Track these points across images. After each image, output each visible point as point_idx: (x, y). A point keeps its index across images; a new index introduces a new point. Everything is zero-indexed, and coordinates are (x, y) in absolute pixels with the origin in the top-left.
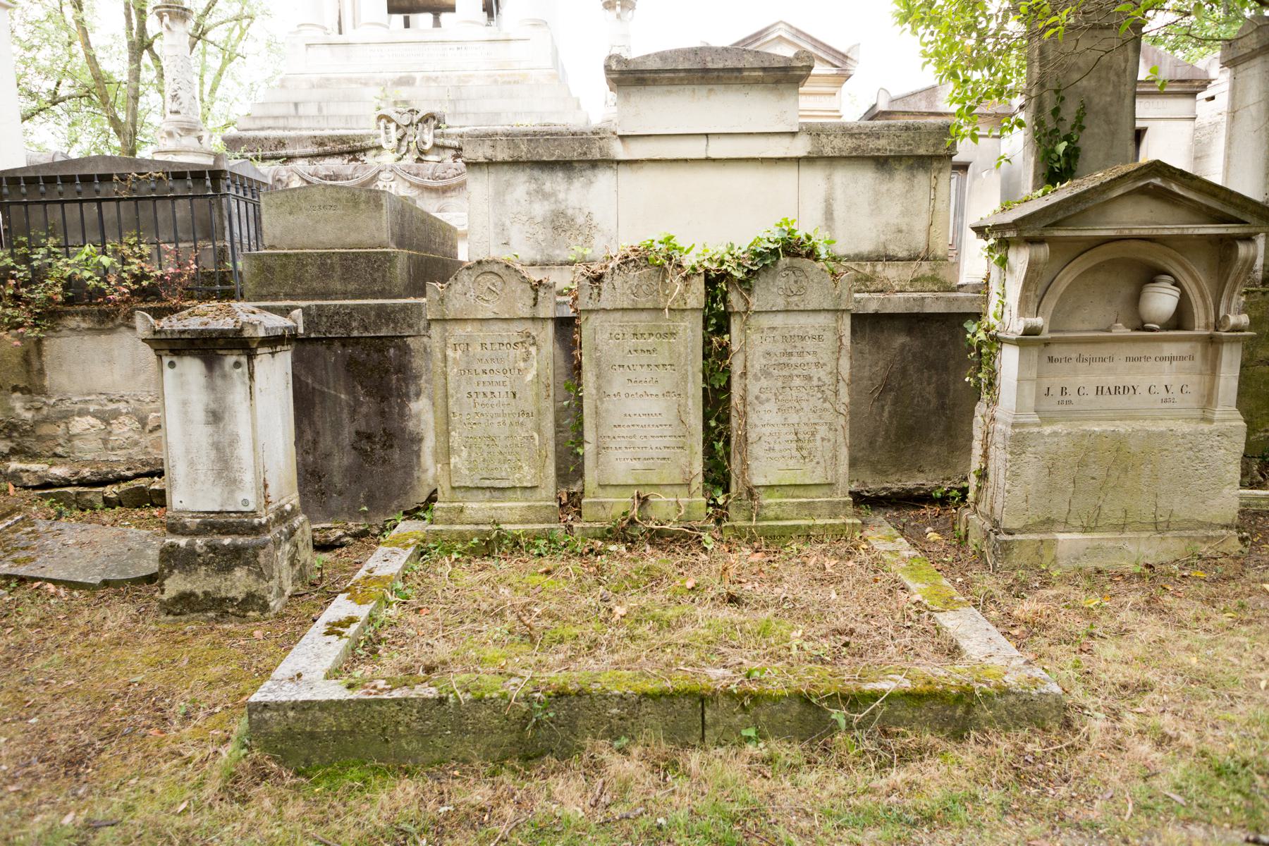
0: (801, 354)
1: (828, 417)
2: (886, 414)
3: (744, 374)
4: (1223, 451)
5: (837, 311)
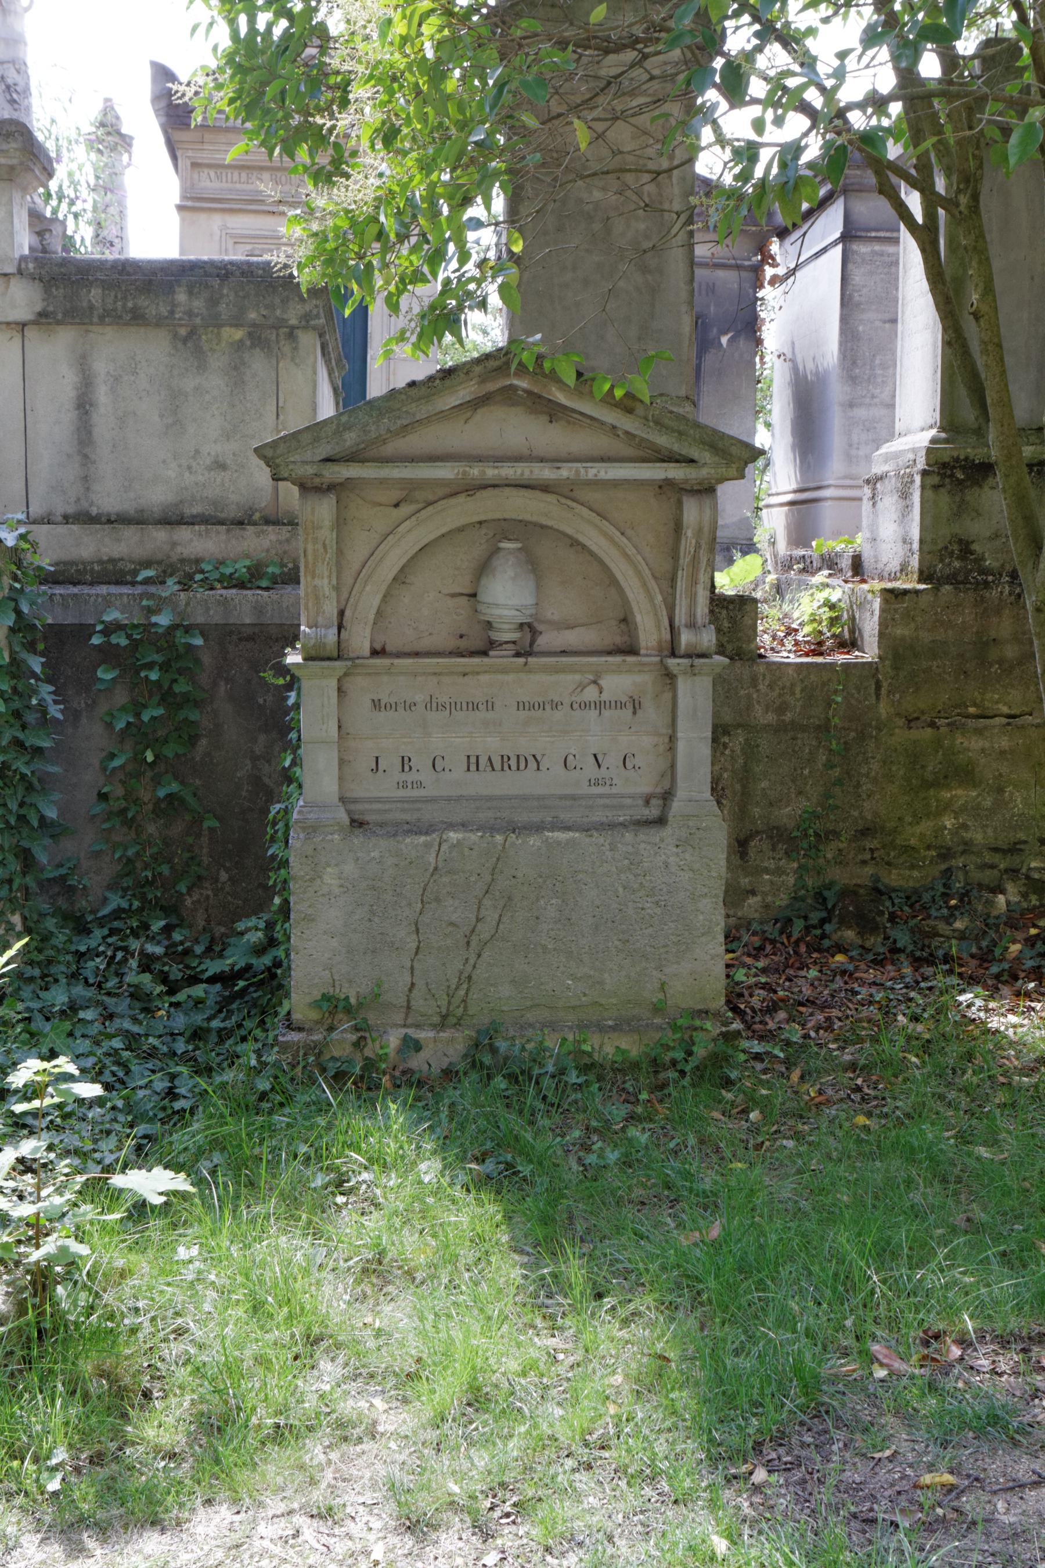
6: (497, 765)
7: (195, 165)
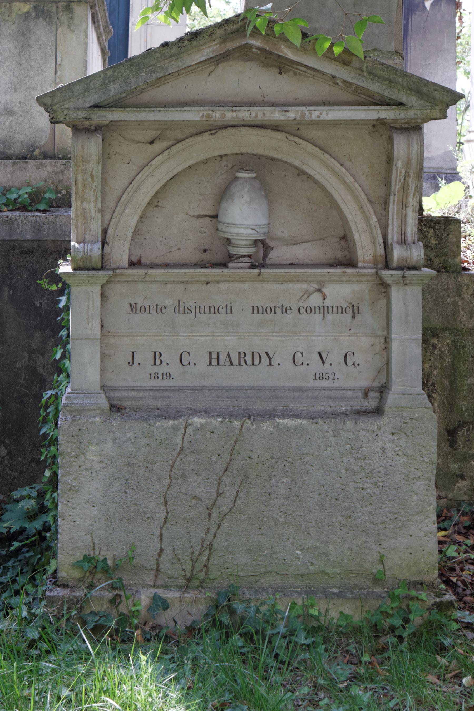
6: (235, 361)
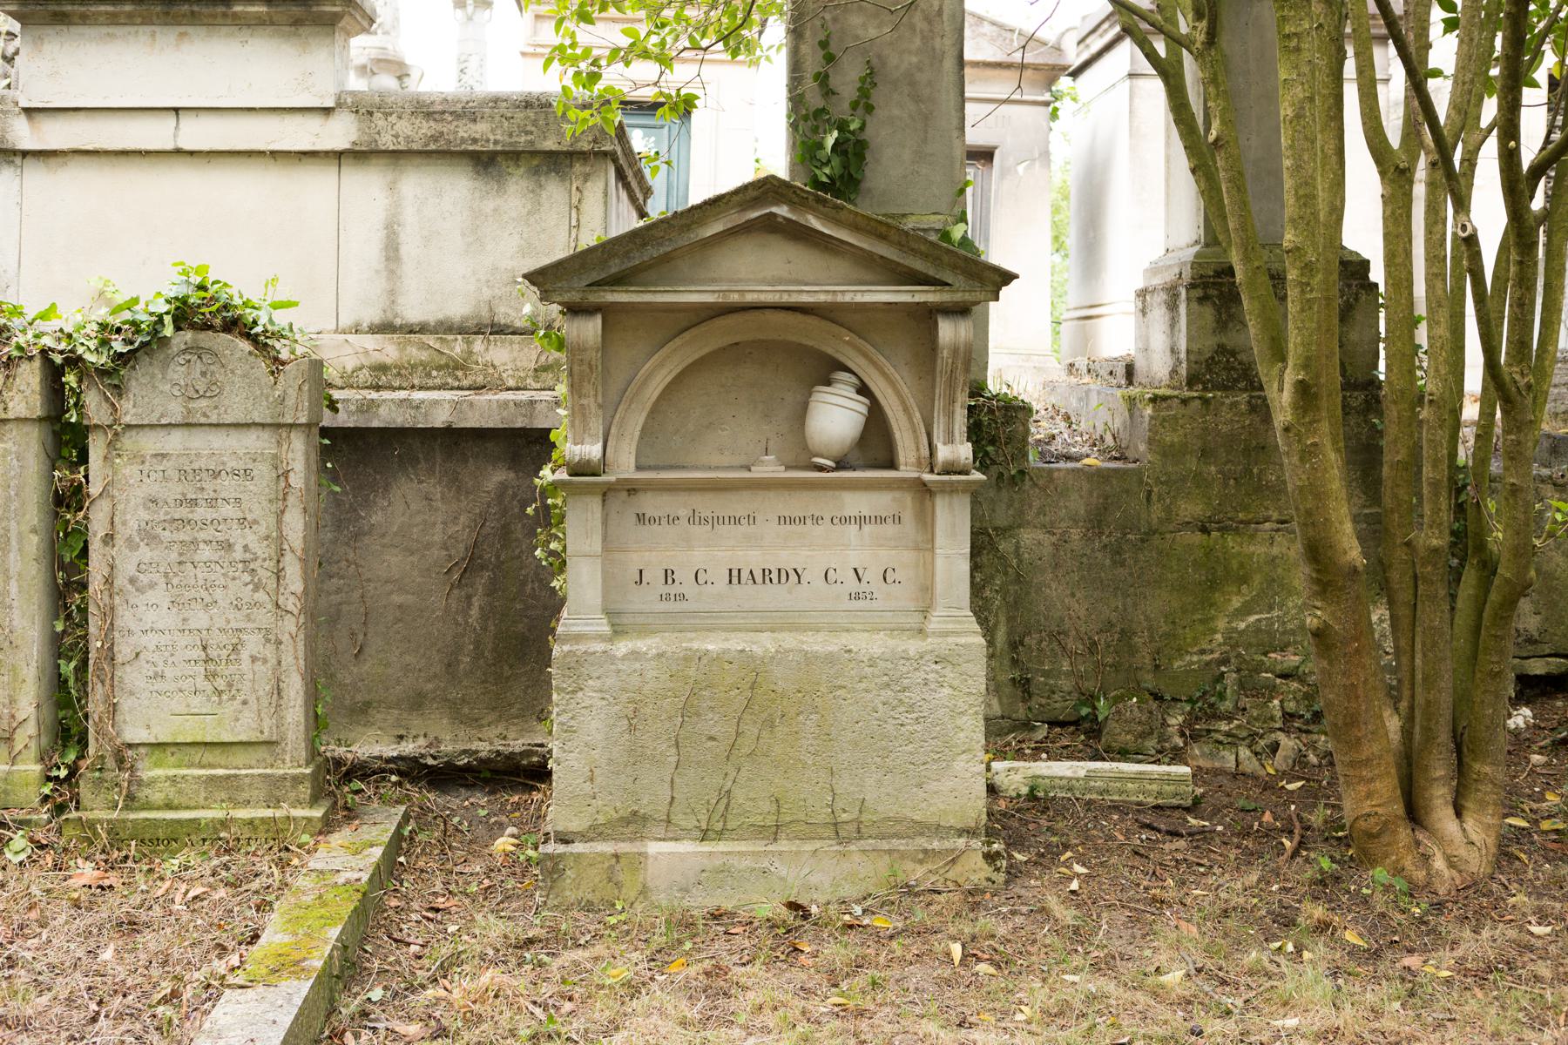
0: (212, 503)
1: (264, 617)
2: (475, 612)
3: (109, 539)
4: (946, 691)
5: (279, 426)
6: (759, 578)
7: (538, 17)
